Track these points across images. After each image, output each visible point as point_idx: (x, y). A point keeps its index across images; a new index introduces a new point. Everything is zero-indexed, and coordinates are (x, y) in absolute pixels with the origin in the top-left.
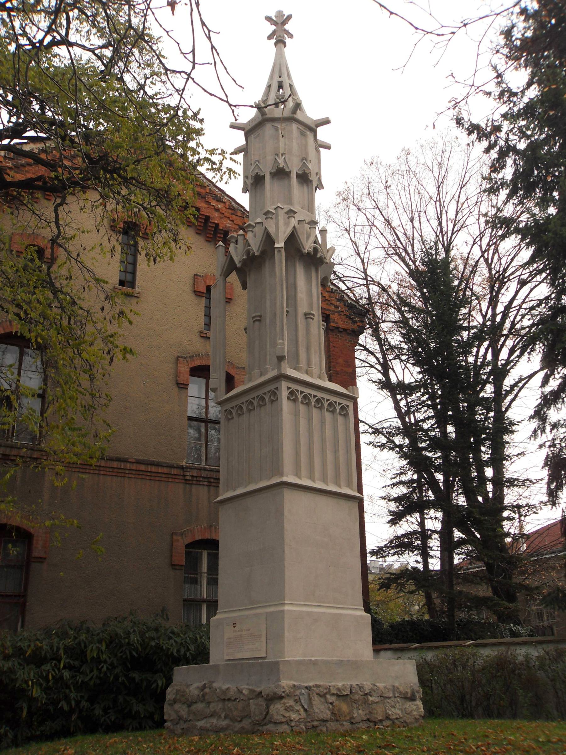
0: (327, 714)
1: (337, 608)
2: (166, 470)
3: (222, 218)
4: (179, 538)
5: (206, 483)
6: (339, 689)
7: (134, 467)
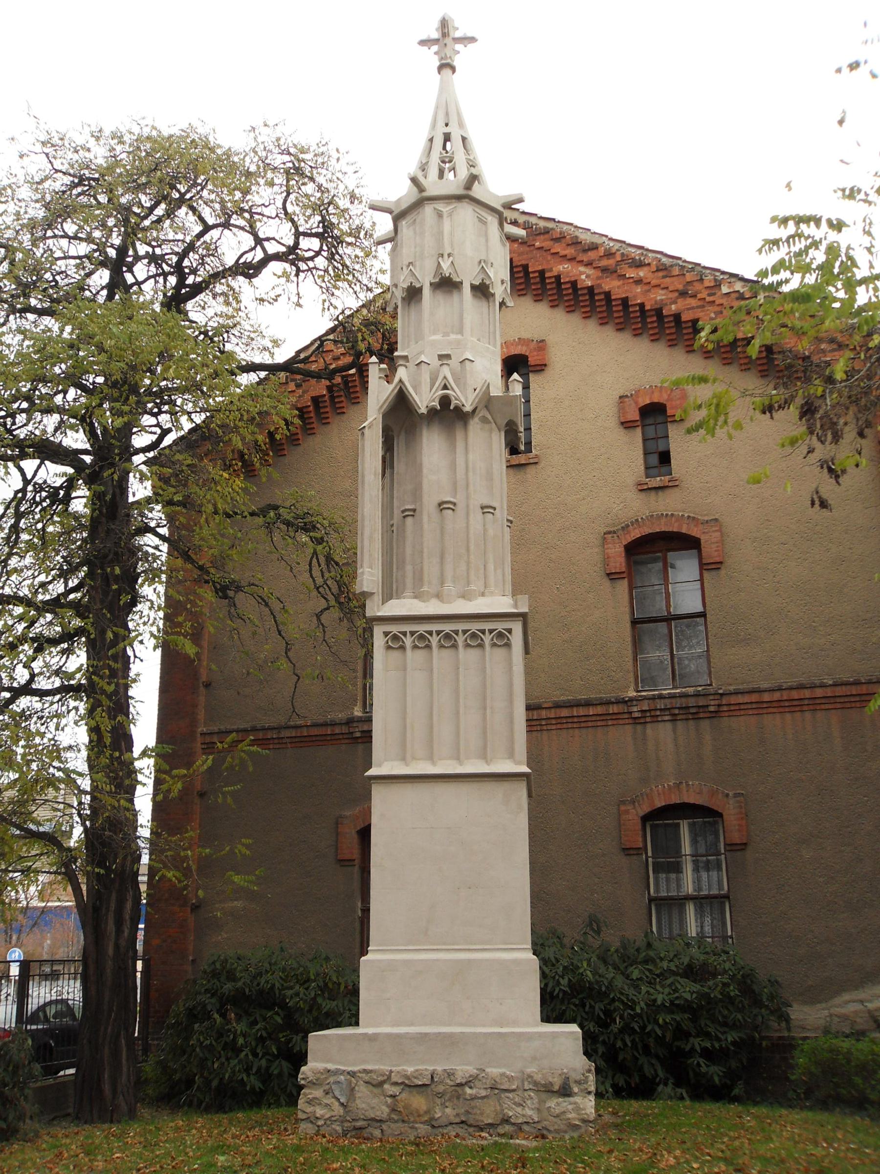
0: (383, 1111)
1: (469, 950)
2: (600, 710)
3: (649, 291)
4: (629, 807)
5: (667, 718)
6: (408, 1078)
7: (552, 714)
